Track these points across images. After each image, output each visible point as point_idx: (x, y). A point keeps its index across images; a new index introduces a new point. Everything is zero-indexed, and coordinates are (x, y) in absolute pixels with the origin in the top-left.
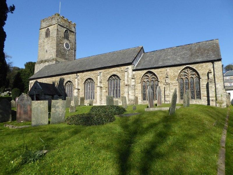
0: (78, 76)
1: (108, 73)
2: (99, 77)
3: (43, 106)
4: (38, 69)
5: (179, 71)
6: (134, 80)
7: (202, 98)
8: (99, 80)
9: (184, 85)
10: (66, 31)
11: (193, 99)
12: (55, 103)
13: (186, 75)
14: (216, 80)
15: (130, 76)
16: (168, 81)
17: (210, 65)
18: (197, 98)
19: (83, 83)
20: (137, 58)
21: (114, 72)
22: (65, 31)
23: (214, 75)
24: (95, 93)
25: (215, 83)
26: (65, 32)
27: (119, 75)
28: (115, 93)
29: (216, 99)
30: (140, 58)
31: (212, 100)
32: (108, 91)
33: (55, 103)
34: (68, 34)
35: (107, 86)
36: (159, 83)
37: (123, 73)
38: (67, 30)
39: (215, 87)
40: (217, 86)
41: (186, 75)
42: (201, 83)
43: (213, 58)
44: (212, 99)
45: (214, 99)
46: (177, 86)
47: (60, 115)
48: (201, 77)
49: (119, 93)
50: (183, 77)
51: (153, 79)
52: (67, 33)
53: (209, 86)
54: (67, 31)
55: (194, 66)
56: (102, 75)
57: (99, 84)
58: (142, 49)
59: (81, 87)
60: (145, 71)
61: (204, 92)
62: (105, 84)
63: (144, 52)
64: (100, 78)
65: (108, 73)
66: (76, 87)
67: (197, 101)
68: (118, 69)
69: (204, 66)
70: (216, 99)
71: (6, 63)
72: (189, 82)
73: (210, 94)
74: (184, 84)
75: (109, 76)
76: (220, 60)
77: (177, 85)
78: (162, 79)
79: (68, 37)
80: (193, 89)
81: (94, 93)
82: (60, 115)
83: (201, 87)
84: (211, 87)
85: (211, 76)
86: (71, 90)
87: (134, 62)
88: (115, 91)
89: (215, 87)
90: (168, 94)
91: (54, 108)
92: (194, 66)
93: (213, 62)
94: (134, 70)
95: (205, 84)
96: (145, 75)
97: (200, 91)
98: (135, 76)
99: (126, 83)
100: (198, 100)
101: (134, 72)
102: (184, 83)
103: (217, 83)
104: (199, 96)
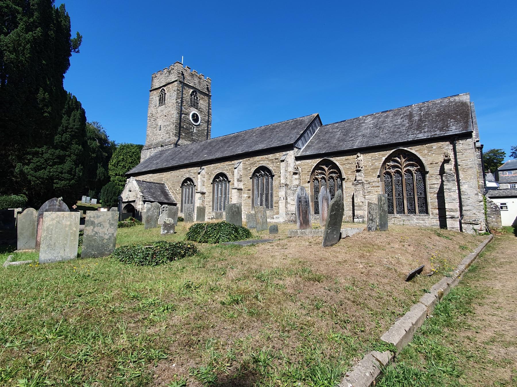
0: (203, 169)
1: (254, 163)
2: (236, 170)
3: (68, 223)
4: (145, 155)
5: (384, 158)
6: (297, 176)
7: (430, 212)
8: (236, 176)
9: (394, 186)
10: (193, 92)
11: (412, 213)
12: (92, 216)
13: (398, 167)
14: (461, 176)
15: (291, 169)
16: (360, 177)
17: (447, 147)
18: (420, 212)
19: (211, 181)
20: (306, 135)
21: (262, 162)
22: (191, 92)
23: (456, 165)
24: (230, 200)
25: (458, 181)
26: (191, 95)
27: (271, 167)
28: (264, 199)
29: (462, 215)
30: (312, 135)
31: (452, 217)
32: (251, 197)
33: (92, 216)
34: (197, 98)
35: (251, 187)
36: (344, 182)
37: (278, 163)
38: (195, 91)
39: (459, 189)
40: (463, 188)
41: (398, 167)
42: (428, 182)
43: (454, 130)
44: (452, 214)
45: (457, 214)
46: (380, 188)
47: (105, 241)
48: (428, 169)
49: (218, 200)
50: (392, 171)
51: (334, 175)
52: (194, 97)
53: (445, 187)
54: (196, 93)
55: (413, 150)
56: (241, 167)
57: (236, 184)
58: (318, 119)
59: (208, 189)
60: (319, 160)
61: (432, 200)
62: (248, 183)
63: (322, 124)
64: (238, 173)
65: (252, 164)
66: (199, 190)
67: (421, 217)
68: (271, 156)
69: (434, 148)
70: (462, 215)
71: (461, 140)
72: (404, 180)
73: (446, 205)
74: (394, 184)
75: (253, 170)
76: (468, 135)
77: (378, 185)
78: (349, 175)
79: (198, 103)
80: (412, 194)
81: (228, 200)
82: (105, 241)
83: (428, 190)
84: (449, 189)
85: (449, 167)
86: (192, 193)
87: (300, 142)
88: (264, 196)
89: (459, 189)
90: (361, 204)
91: (92, 227)
92: (413, 150)
93: (453, 139)
94: (297, 159)
95: (437, 184)
96: (317, 167)
97: (425, 198)
98: (300, 169)
99: (283, 181)
100: (423, 216)
101: (298, 162)
102: (393, 181)
103: (464, 181)
104: (425, 211)
